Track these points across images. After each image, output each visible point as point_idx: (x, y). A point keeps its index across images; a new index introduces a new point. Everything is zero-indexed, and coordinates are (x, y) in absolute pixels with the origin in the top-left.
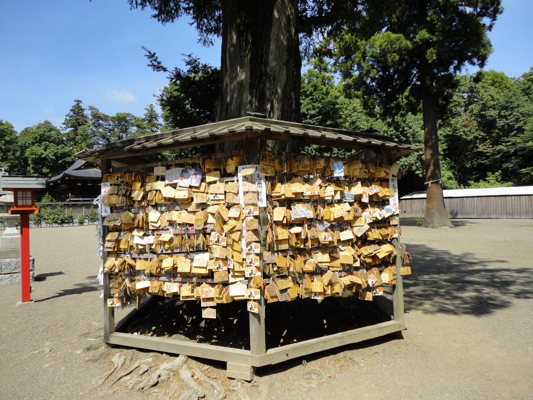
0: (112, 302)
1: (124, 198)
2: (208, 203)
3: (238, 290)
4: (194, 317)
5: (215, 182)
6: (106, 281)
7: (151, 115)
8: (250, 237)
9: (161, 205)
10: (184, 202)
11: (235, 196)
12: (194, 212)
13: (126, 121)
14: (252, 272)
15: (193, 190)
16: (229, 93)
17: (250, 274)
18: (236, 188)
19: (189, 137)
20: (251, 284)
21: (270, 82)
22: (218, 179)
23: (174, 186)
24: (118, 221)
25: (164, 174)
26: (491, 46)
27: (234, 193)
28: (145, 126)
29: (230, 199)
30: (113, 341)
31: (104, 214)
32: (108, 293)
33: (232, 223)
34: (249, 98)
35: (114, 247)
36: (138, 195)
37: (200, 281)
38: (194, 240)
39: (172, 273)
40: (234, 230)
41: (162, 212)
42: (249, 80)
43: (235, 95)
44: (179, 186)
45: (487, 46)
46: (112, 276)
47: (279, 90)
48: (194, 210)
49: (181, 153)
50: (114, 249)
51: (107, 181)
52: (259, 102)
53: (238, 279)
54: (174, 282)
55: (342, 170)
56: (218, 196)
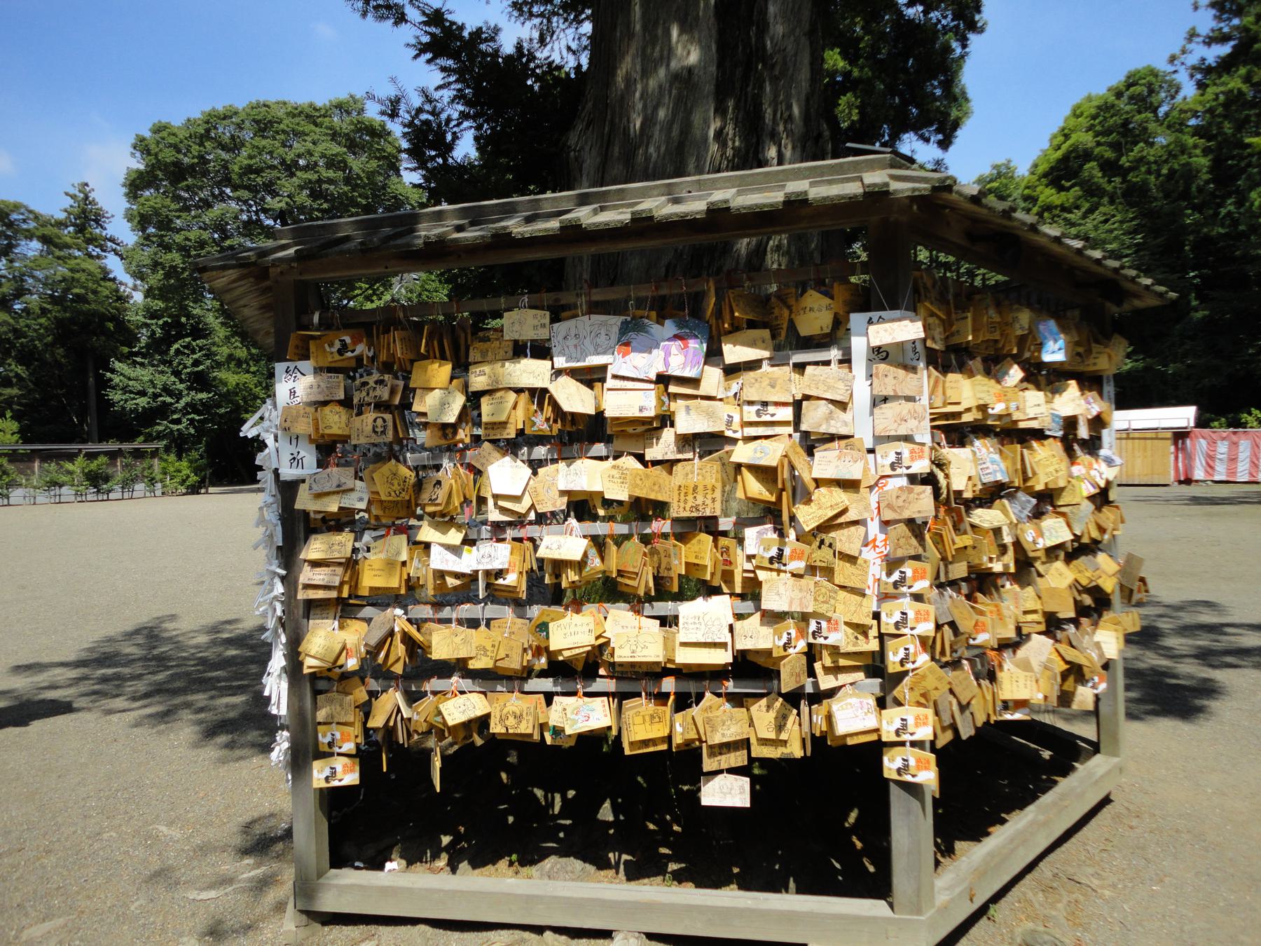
0: (327, 772)
1: (388, 417)
2: (728, 433)
3: (853, 715)
4: (571, 794)
5: (753, 365)
6: (301, 699)
7: (84, 211)
8: (902, 541)
9: (540, 440)
10: (630, 430)
11: (838, 412)
12: (669, 465)
13: (10, 225)
14: (907, 655)
15: (673, 389)
16: (639, 106)
17: (902, 663)
18: (841, 385)
19: (629, 216)
20: (902, 691)
21: (775, 80)
22: (766, 354)
23: (592, 377)
24: (354, 495)
25: (542, 334)
26: (967, 100)
27: (832, 402)
28: (68, 240)
29: (815, 419)
30: (329, 903)
31: (288, 473)
32: (311, 741)
33: (826, 503)
34: (715, 125)
35: (342, 583)
36: (443, 405)
37: (692, 687)
38: (653, 554)
39: (574, 672)
40: (841, 520)
41: (535, 465)
42: (713, 69)
43: (662, 114)
44: (615, 377)
45: (954, 97)
46: (322, 685)
47: (796, 110)
48: (671, 456)
49: (179, 317)
50: (340, 591)
51: (307, 358)
52: (744, 139)
53: (844, 678)
54: (587, 695)
55: (1061, 343)
56: (771, 409)
